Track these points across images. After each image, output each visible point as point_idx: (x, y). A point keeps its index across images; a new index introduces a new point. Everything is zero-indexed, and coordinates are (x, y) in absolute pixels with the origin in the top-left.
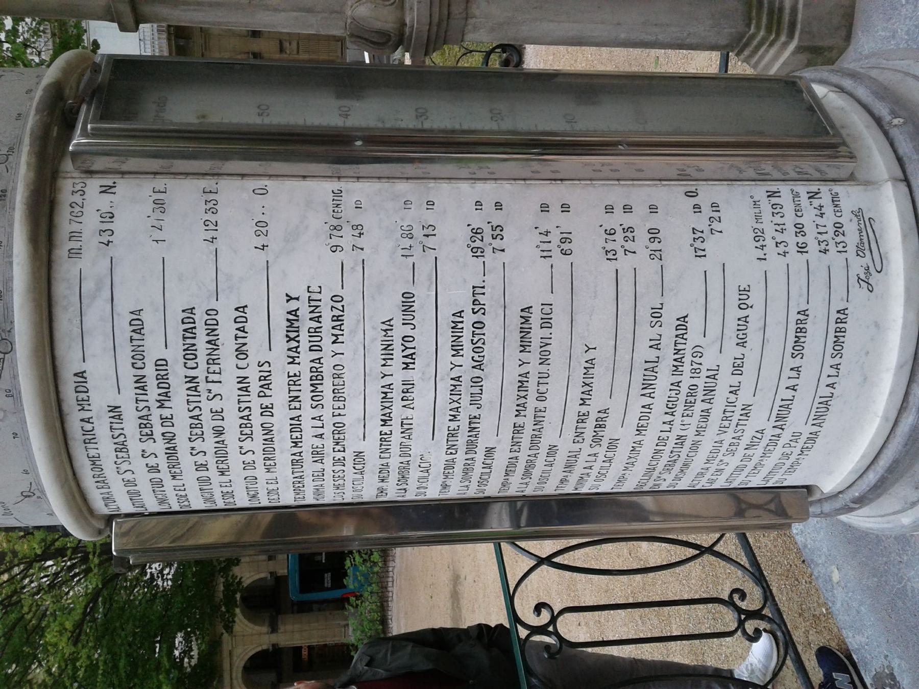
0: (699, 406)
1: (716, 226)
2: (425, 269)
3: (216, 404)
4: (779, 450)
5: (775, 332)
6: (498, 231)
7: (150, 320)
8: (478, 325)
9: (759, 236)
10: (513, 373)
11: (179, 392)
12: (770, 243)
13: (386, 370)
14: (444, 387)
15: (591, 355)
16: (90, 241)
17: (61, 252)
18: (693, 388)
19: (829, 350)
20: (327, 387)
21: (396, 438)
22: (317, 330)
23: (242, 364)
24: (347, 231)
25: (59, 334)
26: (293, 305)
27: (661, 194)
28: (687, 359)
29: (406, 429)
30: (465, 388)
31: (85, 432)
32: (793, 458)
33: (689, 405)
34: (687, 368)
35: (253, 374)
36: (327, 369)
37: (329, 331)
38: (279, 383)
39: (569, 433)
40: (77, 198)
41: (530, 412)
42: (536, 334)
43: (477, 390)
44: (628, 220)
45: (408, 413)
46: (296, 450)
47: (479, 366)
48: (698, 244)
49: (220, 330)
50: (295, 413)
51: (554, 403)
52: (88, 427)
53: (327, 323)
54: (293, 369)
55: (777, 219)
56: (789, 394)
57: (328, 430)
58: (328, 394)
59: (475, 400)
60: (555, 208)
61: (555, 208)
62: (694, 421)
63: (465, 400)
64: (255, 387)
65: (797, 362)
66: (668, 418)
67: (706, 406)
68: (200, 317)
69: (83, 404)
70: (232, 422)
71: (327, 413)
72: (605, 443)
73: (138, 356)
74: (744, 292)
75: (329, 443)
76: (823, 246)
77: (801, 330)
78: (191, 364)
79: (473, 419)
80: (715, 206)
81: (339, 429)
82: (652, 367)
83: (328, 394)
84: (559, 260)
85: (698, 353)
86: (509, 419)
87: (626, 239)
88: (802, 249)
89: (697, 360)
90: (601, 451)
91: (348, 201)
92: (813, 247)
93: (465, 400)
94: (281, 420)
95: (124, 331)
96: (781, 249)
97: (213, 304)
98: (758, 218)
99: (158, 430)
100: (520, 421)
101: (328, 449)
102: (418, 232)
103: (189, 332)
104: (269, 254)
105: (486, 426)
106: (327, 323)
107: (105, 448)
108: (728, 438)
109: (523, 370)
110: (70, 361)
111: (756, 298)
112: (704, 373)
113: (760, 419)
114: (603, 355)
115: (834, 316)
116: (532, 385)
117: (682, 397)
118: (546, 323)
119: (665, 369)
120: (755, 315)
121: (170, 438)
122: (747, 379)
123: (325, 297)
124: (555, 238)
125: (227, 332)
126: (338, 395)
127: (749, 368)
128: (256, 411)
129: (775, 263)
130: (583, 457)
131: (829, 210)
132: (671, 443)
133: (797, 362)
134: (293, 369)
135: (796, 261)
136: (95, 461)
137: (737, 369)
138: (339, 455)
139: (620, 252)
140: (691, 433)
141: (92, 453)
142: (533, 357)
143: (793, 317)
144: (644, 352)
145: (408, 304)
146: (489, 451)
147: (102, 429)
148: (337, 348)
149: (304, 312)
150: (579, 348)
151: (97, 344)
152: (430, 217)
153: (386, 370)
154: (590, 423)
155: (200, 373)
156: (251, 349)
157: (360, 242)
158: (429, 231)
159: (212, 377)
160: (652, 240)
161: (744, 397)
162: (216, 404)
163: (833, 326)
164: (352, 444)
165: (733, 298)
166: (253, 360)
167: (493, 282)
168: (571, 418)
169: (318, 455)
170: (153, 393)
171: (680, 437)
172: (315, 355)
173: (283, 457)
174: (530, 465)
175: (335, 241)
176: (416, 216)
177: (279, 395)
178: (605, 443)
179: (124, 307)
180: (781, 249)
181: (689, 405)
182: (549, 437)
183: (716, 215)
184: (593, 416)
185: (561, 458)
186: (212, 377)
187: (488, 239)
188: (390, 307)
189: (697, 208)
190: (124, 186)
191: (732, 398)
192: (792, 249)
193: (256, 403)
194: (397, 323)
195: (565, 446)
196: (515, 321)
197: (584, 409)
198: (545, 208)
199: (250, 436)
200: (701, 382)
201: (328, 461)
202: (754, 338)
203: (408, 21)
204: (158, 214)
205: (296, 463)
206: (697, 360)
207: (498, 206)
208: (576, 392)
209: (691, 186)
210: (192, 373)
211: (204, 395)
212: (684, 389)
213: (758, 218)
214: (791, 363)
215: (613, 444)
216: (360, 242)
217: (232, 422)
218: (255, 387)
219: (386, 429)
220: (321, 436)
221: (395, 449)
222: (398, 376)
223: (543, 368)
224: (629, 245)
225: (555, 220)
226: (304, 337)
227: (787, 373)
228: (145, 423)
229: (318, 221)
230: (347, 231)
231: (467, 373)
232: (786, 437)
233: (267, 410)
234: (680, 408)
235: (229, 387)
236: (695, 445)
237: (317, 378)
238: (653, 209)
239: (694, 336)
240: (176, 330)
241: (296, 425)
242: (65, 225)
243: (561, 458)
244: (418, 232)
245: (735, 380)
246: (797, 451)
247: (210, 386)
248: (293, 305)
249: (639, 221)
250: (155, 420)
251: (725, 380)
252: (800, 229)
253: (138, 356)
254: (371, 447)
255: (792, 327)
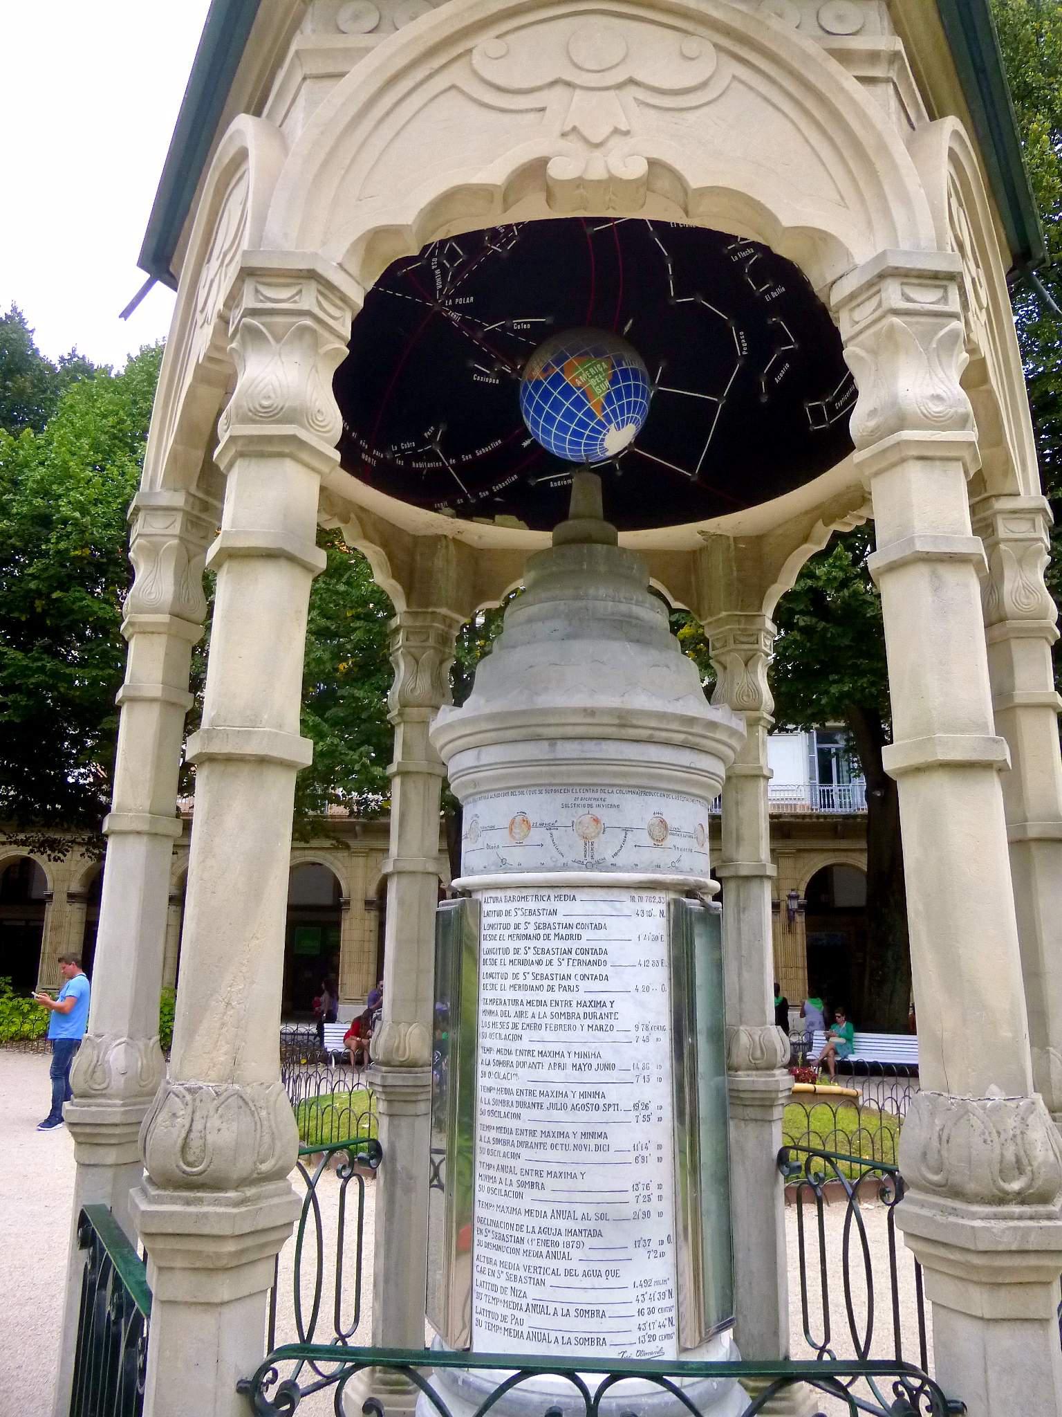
0: (544, 1250)
1: (652, 1254)
2: (628, 1076)
3: (555, 962)
4: (508, 1312)
5: (591, 1296)
6: (647, 1118)
7: (601, 934)
8: (597, 1107)
9: (647, 1283)
10: (569, 1128)
11: (564, 945)
12: (643, 1290)
13: (572, 1055)
14: (561, 1088)
15: (579, 1176)
16: (638, 906)
17: (633, 893)
18: (557, 1244)
19: (580, 1335)
20: (563, 1021)
21: (529, 1059)
22: (595, 1017)
23: (578, 977)
24: (646, 1033)
25: (595, 890)
26: (608, 1005)
27: (668, 1219)
28: (575, 1239)
29: (533, 1066)
30: (560, 1100)
31: (542, 897)
32: (503, 1325)
33: (546, 1243)
34: (570, 1239)
35: (572, 982)
36: (573, 1022)
37: (940, 1053)
38: (567, 996)
39: (529, 1166)
40: (657, 900)
41: (544, 1140)
42: (592, 1142)
43: (559, 1107)
44: (654, 1198)
45: (546, 1066)
46: (525, 1002)
47: (574, 1108)
48: (642, 1243)
49: (596, 967)
50: (548, 1003)
51: (550, 1155)
52: (545, 899)
53: (599, 1022)
54: (574, 1004)
55: (657, 1296)
56: (551, 1311)
57: (537, 1020)
58: (558, 1022)
59: (553, 1106)
60: (659, 1153)
61: (659, 1153)
62: (535, 1248)
63: (553, 1100)
64: (564, 983)
65: (573, 1313)
66: (537, 1230)
67: (544, 1254)
68: (602, 957)
69: (558, 897)
70: (544, 970)
71: (548, 1021)
72: (521, 1190)
73: (583, 926)
74: (615, 1274)
75: (528, 1021)
76: (643, 1327)
77: (592, 1314)
78: (578, 951)
79: (540, 1106)
80: (662, 1255)
81: (538, 1027)
82: (570, 1215)
83: (558, 1022)
84: (631, 1157)
85: (580, 1245)
86: (539, 1127)
87: (644, 1196)
88: (640, 1312)
89: (575, 1245)
90: (515, 1188)
91: (660, 1034)
92: (642, 1320)
93: (553, 1100)
94: (545, 996)
95: (597, 920)
96: (641, 1298)
97: (609, 964)
98: (657, 1283)
99: (542, 932)
100: (538, 1134)
101: (524, 1020)
102: (646, 1073)
103: (595, 952)
104: (634, 993)
105: (536, 1113)
106: (599, 1022)
107: (532, 905)
108: (522, 1273)
109: (571, 1135)
110: (580, 894)
111: (613, 1282)
112: (566, 1251)
113: (533, 1292)
114: (580, 1184)
115: (601, 1336)
116: (560, 1140)
117: (551, 1238)
118: (598, 1148)
119: (569, 1224)
120: (601, 1282)
121: (537, 937)
122: (562, 1280)
123: (612, 1022)
124: (645, 1153)
125: (595, 970)
126: (558, 1027)
127: (571, 1281)
128: (551, 983)
129: (631, 1294)
130: (510, 1176)
131: (663, 1331)
132: (519, 1234)
133: (573, 1313)
134: (574, 1004)
135: (635, 1307)
136: (525, 898)
137: (569, 1273)
138: (520, 1026)
139: (637, 1193)
140: (526, 1246)
141: (530, 898)
142: (578, 1141)
143: (601, 1308)
144: (580, 1210)
145: (608, 1067)
146: (518, 1116)
147: (542, 905)
148: (586, 1027)
149: (605, 1010)
150: (582, 1168)
151: (590, 907)
152: (653, 1079)
153: (572, 1055)
154: (535, 1179)
155: (573, 956)
156: (586, 982)
157: (640, 1040)
158: (646, 1079)
159: (571, 961)
160: (644, 1213)
161: (550, 1280)
162: (555, 962)
163: (595, 1336)
164: (527, 1035)
165: (612, 1266)
166: (580, 983)
167: (619, 1116)
168: (538, 1167)
169: (520, 1014)
170: (563, 932)
171: (522, 1240)
172: (582, 1016)
173: (519, 995)
174: (506, 1143)
175: (641, 1027)
176: (654, 1072)
177: (560, 995)
178: (521, 1190)
179: (607, 921)
180: (641, 1298)
181: (546, 1243)
182: (525, 1153)
183: (658, 1255)
184: (540, 1180)
185: (510, 1162)
186: (571, 961)
187: (644, 1113)
188: (608, 1057)
189: (662, 1242)
190: (663, 921)
191: (550, 1272)
192: (641, 1306)
193: (556, 983)
194: (599, 1061)
195: (518, 1164)
196: (599, 1129)
197: (544, 1174)
198: (660, 1147)
199: (536, 978)
200: (560, 1249)
201: (516, 1020)
202: (587, 1282)
203: (739, 1073)
204: (651, 937)
205: (515, 1002)
206: (575, 1245)
207: (660, 1119)
208: (556, 1168)
209: (673, 1239)
210: (573, 952)
211: (562, 957)
212: (556, 1238)
213: (657, 1283)
214: (572, 1308)
215: (519, 1195)
216: (640, 1040)
217: (544, 970)
218: (564, 983)
219: (536, 1053)
220: (533, 1016)
221: (522, 1059)
222: (568, 1061)
223: (572, 1147)
224: (641, 1199)
225: (653, 1153)
226: (591, 1010)
227: (566, 1307)
228: (546, 926)
229: (651, 1018)
230: (646, 1033)
231: (570, 1101)
232: (519, 1315)
233: (551, 988)
234: (543, 1237)
235: (564, 970)
236: (516, 1251)
237: (569, 1016)
238: (660, 1214)
239: (590, 1241)
240: (596, 945)
241: (541, 1003)
242: (645, 894)
243: (510, 1162)
244: (646, 1073)
245: (561, 1272)
246: (508, 1326)
247: (566, 961)
248: (608, 1005)
249: (655, 1206)
250: (547, 931)
251: (562, 1265)
252: (652, 1311)
253: (583, 926)
254: (524, 1044)
255: (595, 1308)
